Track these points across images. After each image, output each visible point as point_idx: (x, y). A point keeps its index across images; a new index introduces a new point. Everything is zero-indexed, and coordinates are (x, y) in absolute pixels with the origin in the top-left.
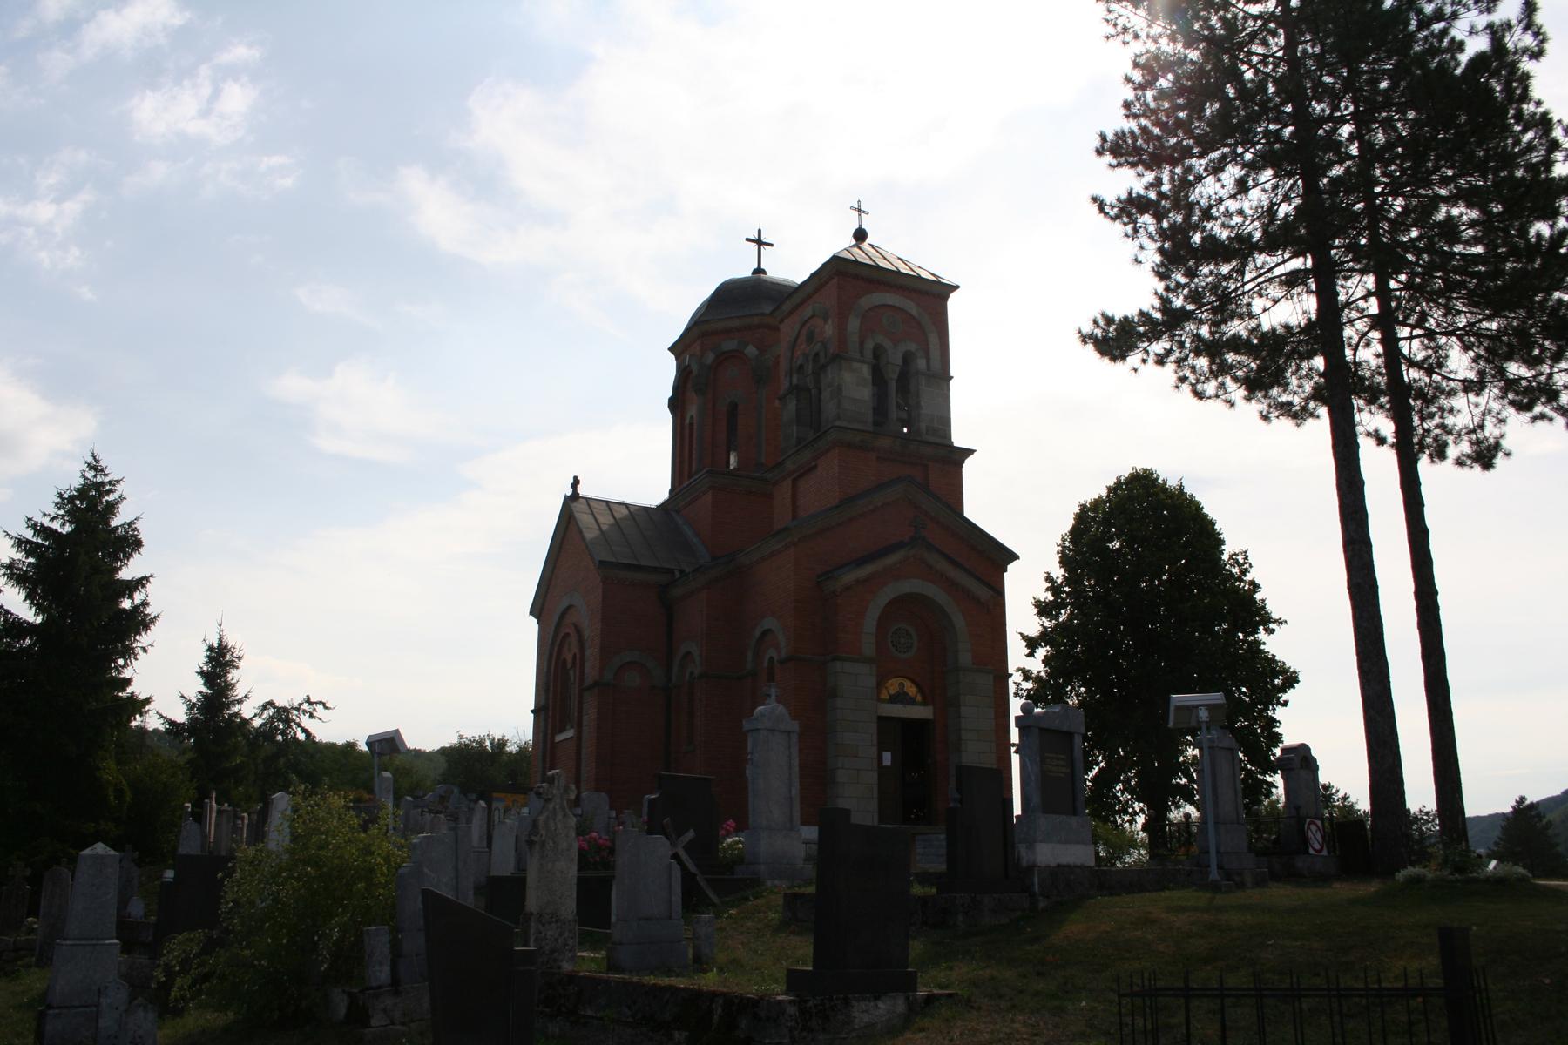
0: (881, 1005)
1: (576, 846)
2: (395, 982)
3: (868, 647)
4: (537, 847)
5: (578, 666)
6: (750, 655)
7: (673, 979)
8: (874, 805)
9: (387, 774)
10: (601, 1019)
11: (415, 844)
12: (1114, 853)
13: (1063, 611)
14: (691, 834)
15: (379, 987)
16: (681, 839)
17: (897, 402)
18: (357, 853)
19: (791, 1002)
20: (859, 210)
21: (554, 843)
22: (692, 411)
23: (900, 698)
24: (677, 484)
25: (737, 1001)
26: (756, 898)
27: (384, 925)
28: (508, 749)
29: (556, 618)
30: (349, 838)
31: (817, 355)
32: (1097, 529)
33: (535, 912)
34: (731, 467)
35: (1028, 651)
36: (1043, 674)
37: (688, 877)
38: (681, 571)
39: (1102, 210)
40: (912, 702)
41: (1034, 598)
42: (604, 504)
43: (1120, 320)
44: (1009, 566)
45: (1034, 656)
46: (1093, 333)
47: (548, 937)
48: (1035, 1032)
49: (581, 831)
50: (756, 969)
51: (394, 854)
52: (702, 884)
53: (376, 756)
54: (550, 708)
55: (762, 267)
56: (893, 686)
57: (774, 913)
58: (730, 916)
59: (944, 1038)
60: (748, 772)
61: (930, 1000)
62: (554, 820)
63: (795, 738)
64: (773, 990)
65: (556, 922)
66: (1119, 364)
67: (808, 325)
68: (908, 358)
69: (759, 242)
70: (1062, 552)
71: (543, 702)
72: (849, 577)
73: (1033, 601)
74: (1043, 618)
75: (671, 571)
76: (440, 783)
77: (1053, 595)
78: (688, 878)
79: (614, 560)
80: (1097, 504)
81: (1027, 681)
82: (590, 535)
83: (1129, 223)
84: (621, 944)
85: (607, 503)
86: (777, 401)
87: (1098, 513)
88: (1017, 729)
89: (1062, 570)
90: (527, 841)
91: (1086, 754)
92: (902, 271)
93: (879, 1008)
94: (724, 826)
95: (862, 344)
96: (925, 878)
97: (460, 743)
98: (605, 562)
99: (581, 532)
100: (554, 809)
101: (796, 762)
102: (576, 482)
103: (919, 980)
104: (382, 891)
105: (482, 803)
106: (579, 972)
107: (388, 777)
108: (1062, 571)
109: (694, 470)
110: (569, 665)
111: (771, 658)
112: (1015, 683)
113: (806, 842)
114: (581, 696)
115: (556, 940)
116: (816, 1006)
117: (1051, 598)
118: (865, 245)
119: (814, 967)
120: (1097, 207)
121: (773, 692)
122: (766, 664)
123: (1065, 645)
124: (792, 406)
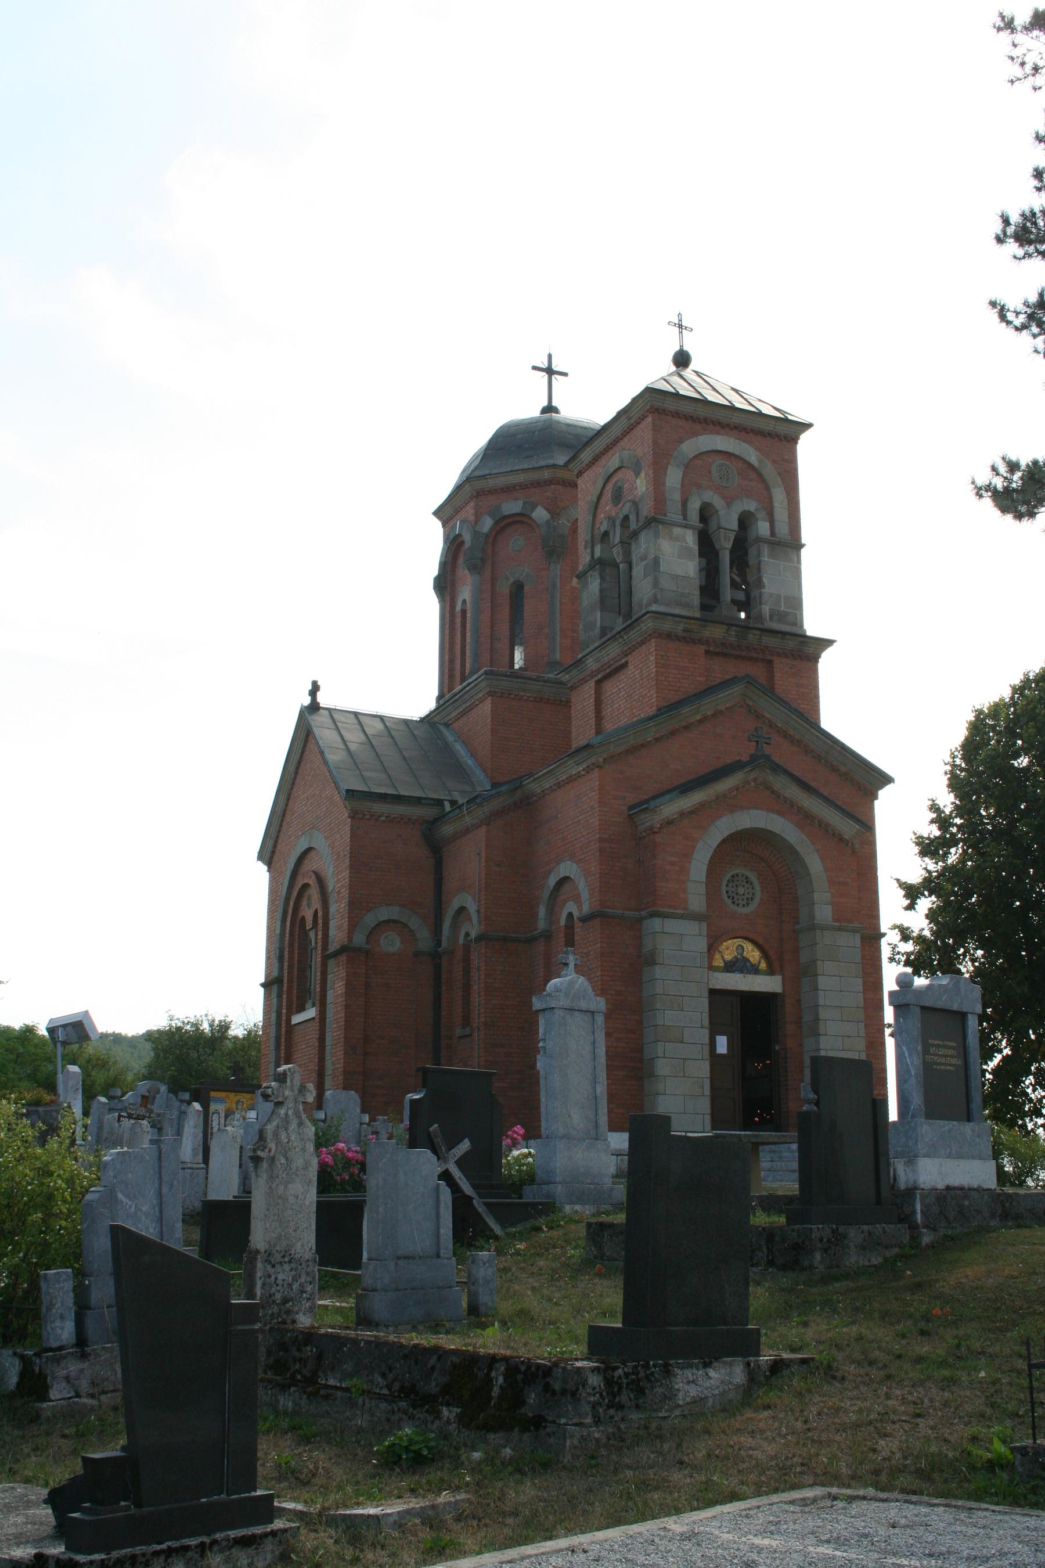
0: (712, 1373)
1: (315, 1162)
2: (81, 1341)
3: (697, 901)
4: (265, 1165)
5: (320, 925)
6: (542, 911)
7: (441, 1336)
8: (704, 1105)
9: (74, 1069)
10: (347, 1390)
11: (106, 1163)
12: (1024, 1165)
13: (953, 850)
14: (465, 1145)
15: (61, 1348)
16: (453, 1151)
17: (732, 579)
18: (32, 1174)
19: (594, 1370)
20: (680, 326)
21: (287, 1159)
22: (465, 594)
23: (738, 965)
24: (446, 690)
25: (523, 1368)
26: (551, 1228)
27: (67, 1267)
28: (232, 1033)
29: (291, 865)
30: (21, 1155)
31: (626, 518)
32: (998, 742)
33: (262, 1250)
34: (517, 667)
35: (907, 902)
36: (927, 933)
37: (461, 1203)
38: (453, 803)
39: (1003, 317)
40: (755, 970)
41: (915, 834)
42: (352, 716)
43: (1028, 465)
44: (880, 792)
45: (915, 909)
46: (990, 483)
47: (279, 1282)
48: (918, 1411)
49: (321, 1142)
50: (550, 1323)
51: (79, 1174)
52: (480, 1210)
53: (59, 1045)
54: (285, 981)
55: (554, 404)
56: (729, 950)
57: (575, 1248)
58: (518, 1253)
59: (797, 1420)
60: (539, 1065)
61: (777, 1367)
62: (286, 1129)
63: (600, 1020)
64: (571, 1352)
65: (290, 1262)
66: (1026, 523)
67: (614, 480)
68: (745, 521)
69: (550, 371)
70: (952, 772)
71: (275, 974)
72: (671, 808)
73: (913, 837)
74: (926, 859)
75: (439, 803)
76: (145, 1078)
77: (940, 829)
78: (461, 1204)
79: (366, 789)
80: (996, 709)
81: (906, 942)
82: (335, 757)
83: (1040, 334)
84: (374, 1290)
85: (356, 714)
86: (575, 580)
87: (998, 720)
88: (892, 1007)
89: (952, 795)
90: (251, 1158)
91: (984, 1037)
92: (737, 405)
93: (710, 1378)
94: (510, 1133)
95: (684, 503)
96: (770, 1203)
97: (170, 1026)
98: (353, 791)
99: (322, 753)
100: (286, 1115)
101: (602, 1051)
102: (315, 689)
103: (763, 1339)
104: (63, 1223)
105: (197, 1106)
106: (319, 1328)
107: (75, 1073)
108: (951, 797)
109: (467, 672)
110: (309, 925)
111: (570, 915)
112: (889, 944)
113: (617, 1154)
114: (324, 965)
115: (290, 1285)
116: (627, 1375)
117: (937, 833)
118: (688, 373)
119: (624, 1322)
120: (997, 315)
121: (571, 959)
122: (563, 922)
123: (955, 894)
124: (594, 585)
